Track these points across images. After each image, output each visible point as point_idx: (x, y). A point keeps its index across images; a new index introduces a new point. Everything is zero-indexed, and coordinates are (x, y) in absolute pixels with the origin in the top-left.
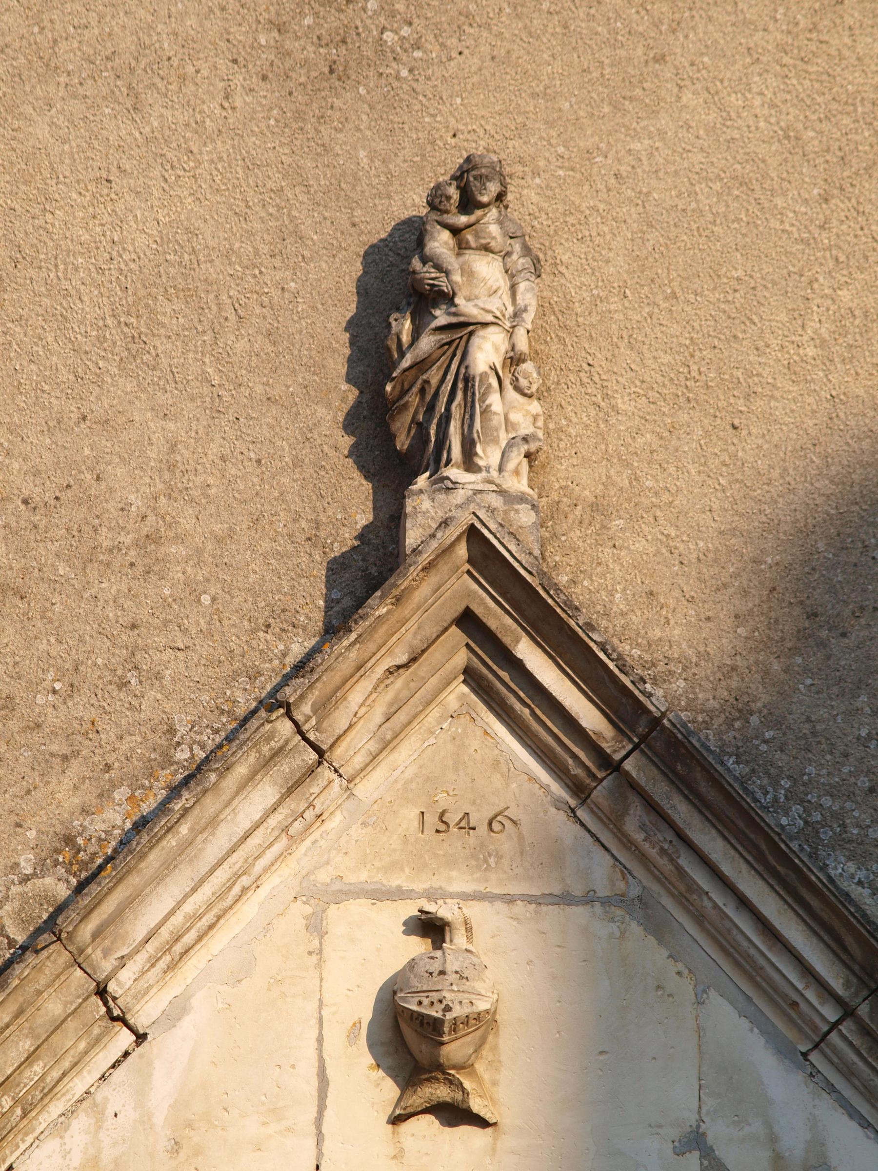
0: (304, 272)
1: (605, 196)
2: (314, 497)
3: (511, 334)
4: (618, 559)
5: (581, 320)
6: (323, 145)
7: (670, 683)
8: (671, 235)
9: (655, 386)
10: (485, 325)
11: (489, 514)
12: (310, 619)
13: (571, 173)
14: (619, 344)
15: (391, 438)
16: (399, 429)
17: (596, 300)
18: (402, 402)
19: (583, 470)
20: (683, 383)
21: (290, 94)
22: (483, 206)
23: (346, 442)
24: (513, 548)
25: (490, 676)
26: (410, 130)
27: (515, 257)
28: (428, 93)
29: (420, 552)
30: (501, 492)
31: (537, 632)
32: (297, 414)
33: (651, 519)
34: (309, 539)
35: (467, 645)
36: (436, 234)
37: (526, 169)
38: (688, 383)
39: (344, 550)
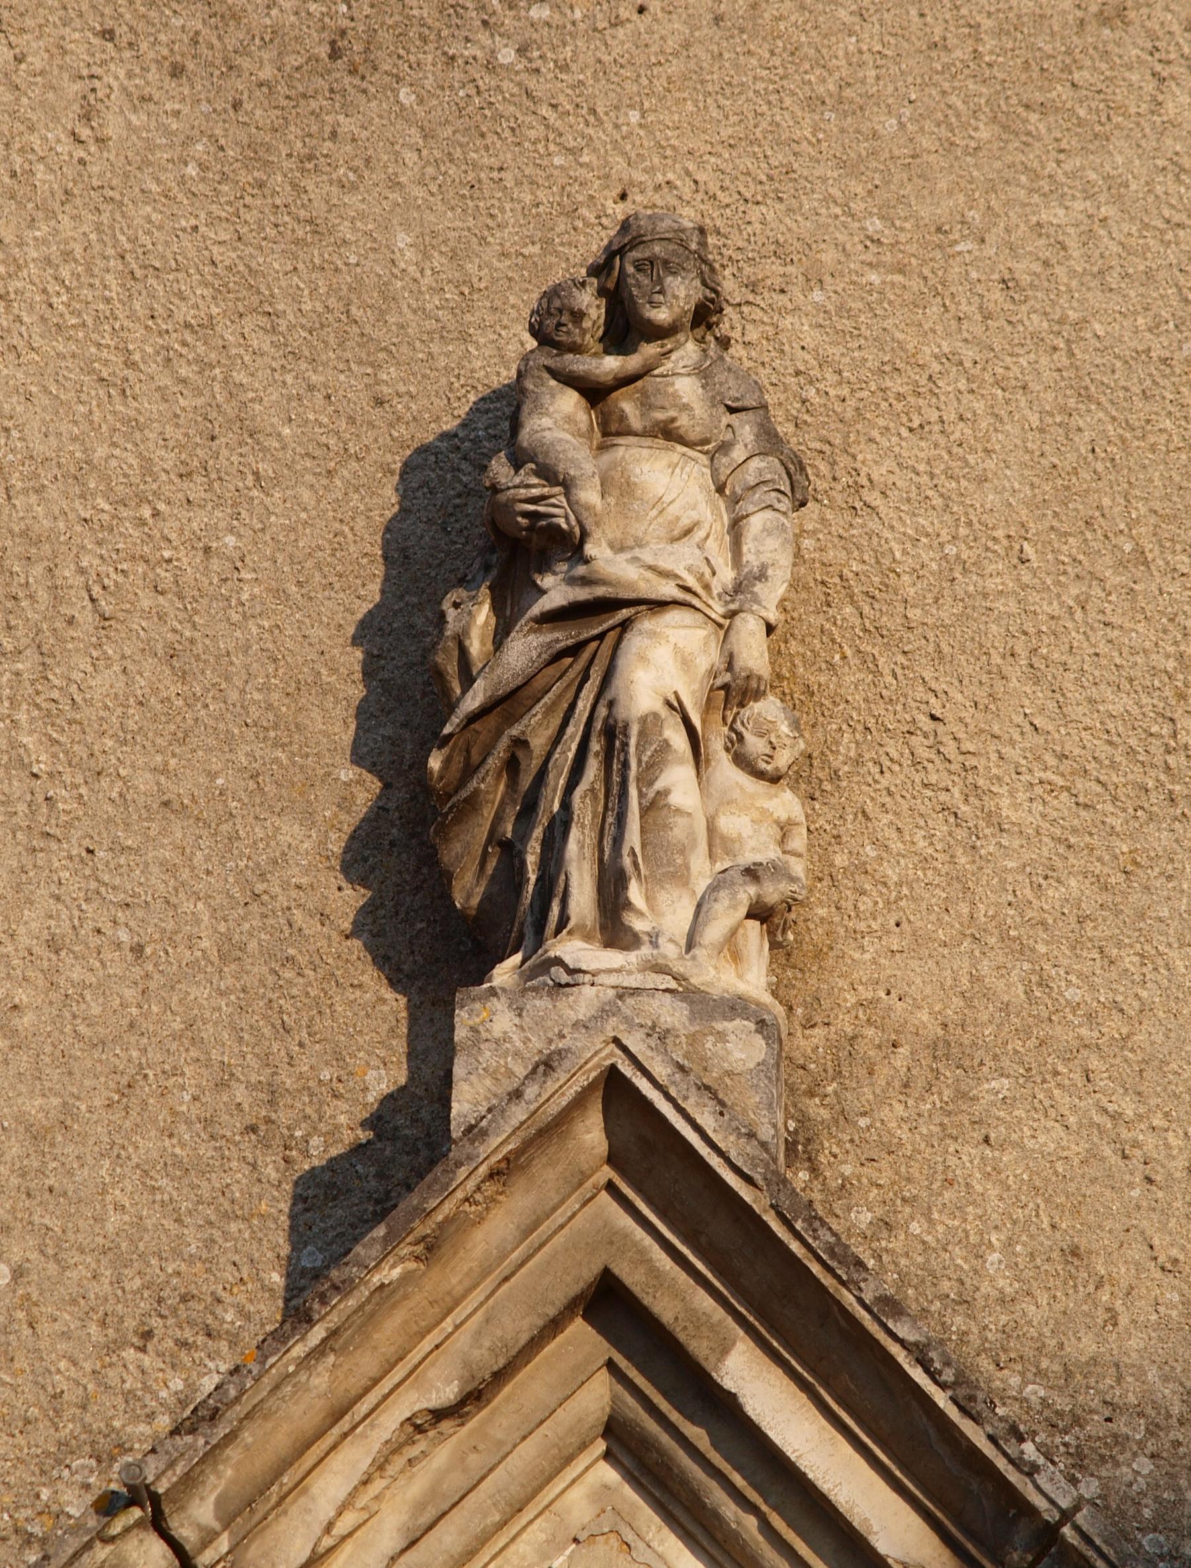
0: (259, 510)
1: (979, 330)
2: (267, 1031)
3: (725, 627)
4: (994, 1172)
5: (915, 614)
6: (310, 221)
7: (1117, 1464)
8: (1133, 419)
9: (1091, 766)
10: (659, 605)
11: (653, 1042)
12: (248, 1317)
13: (898, 278)
14: (1007, 670)
15: (441, 881)
16: (459, 858)
17: (953, 568)
18: (464, 794)
19: (914, 964)
20: (1158, 760)
21: (237, 105)
22: (659, 333)
23: (348, 900)
24: (707, 1120)
25: (665, 1439)
26: (518, 183)
27: (738, 454)
28: (562, 99)
29: (484, 1133)
30: (687, 993)
31: (771, 1328)
32: (234, 837)
33: (1078, 1078)
34: (253, 1129)
35: (611, 1365)
36: (546, 399)
37: (790, 269)
38: (1171, 760)
39: (334, 1152)
